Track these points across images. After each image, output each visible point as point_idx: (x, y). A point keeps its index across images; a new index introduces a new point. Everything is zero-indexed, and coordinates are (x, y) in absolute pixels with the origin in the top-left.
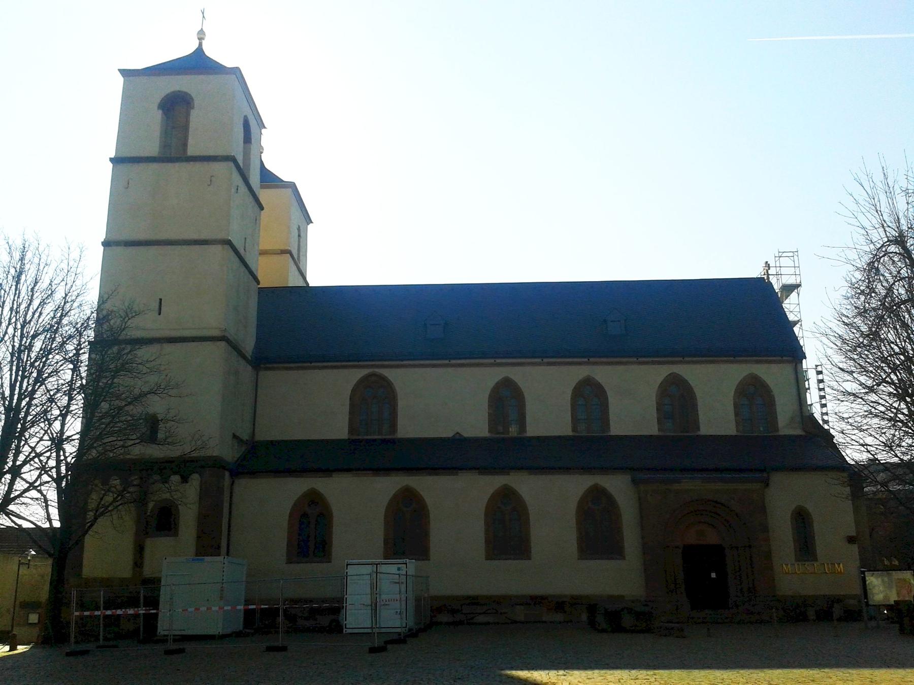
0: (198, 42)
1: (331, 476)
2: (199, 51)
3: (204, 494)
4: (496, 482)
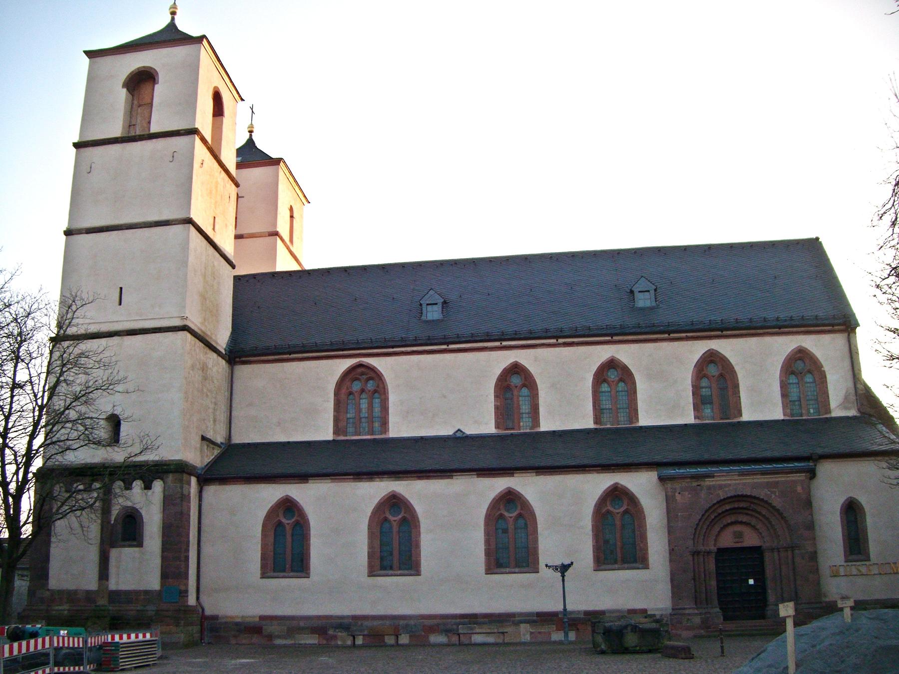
0: (170, 16)
1: (307, 483)
2: (172, 26)
3: (168, 501)
4: (499, 485)
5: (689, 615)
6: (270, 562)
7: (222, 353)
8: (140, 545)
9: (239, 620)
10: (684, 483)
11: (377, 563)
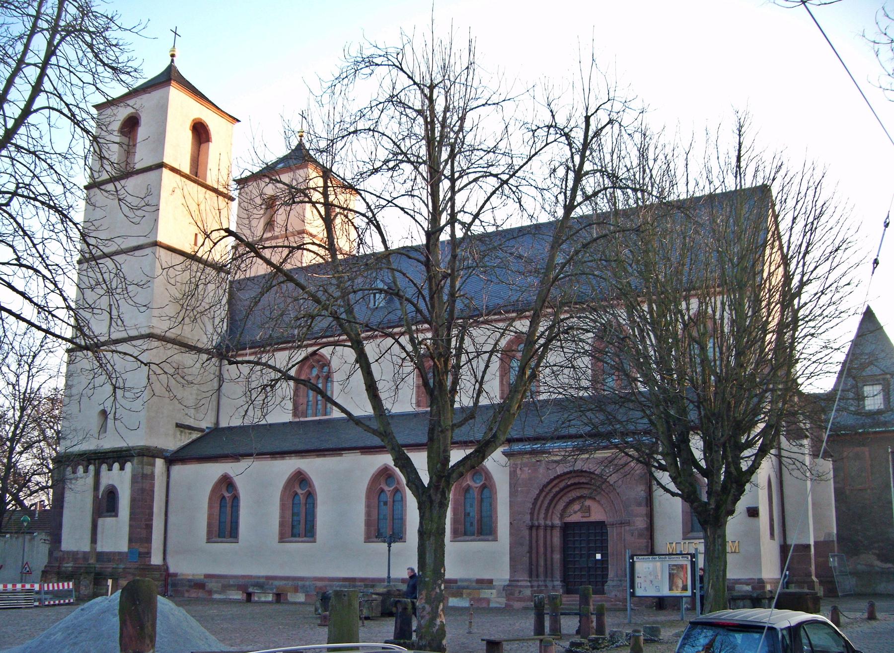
0: (170, 58)
3: (134, 479)
5: (521, 586)
6: (216, 529)
8: (116, 516)
9: (190, 577)
10: (526, 459)
11: (288, 530)
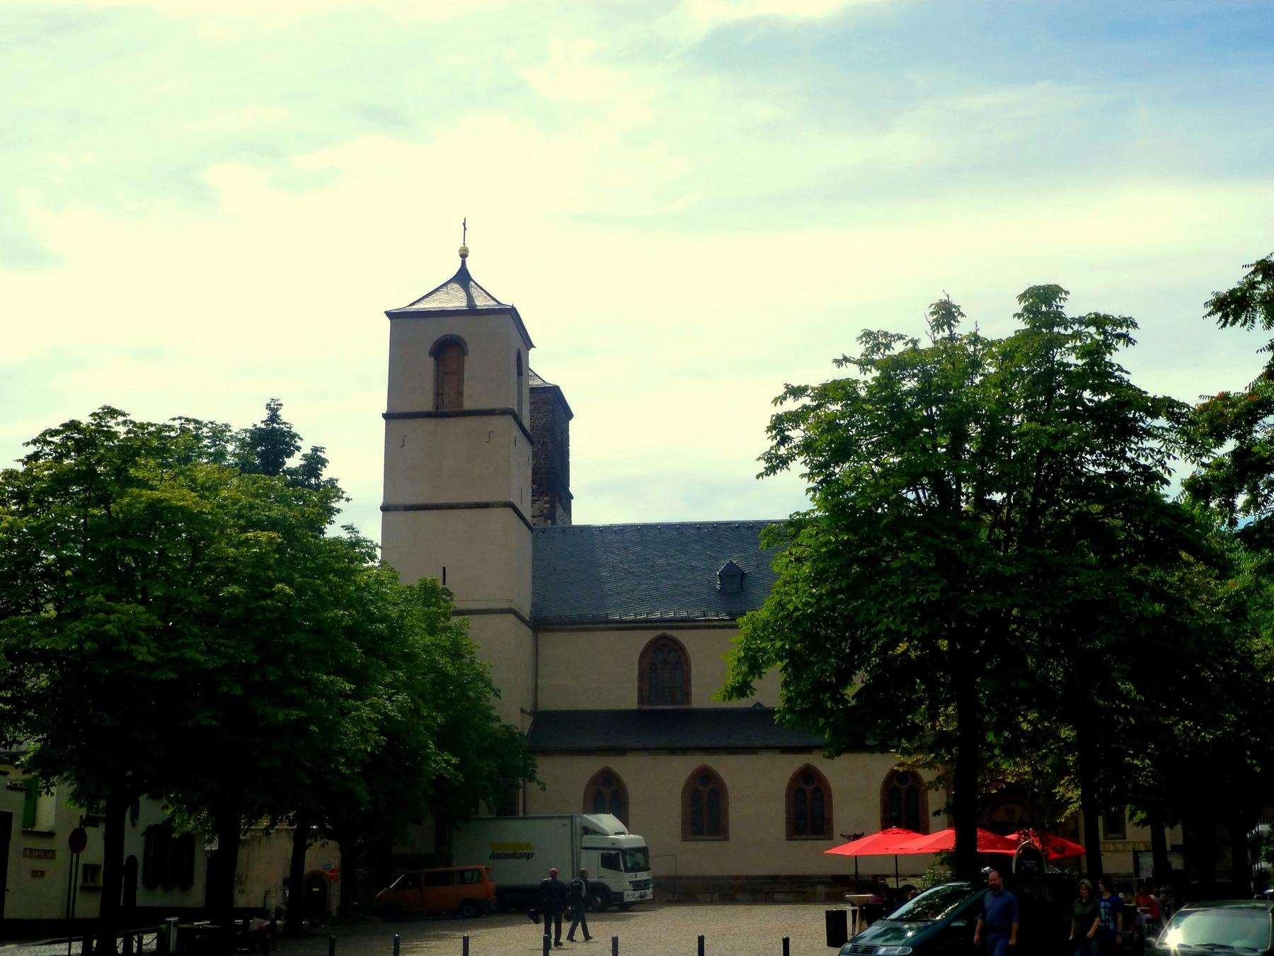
7: (526, 620)
